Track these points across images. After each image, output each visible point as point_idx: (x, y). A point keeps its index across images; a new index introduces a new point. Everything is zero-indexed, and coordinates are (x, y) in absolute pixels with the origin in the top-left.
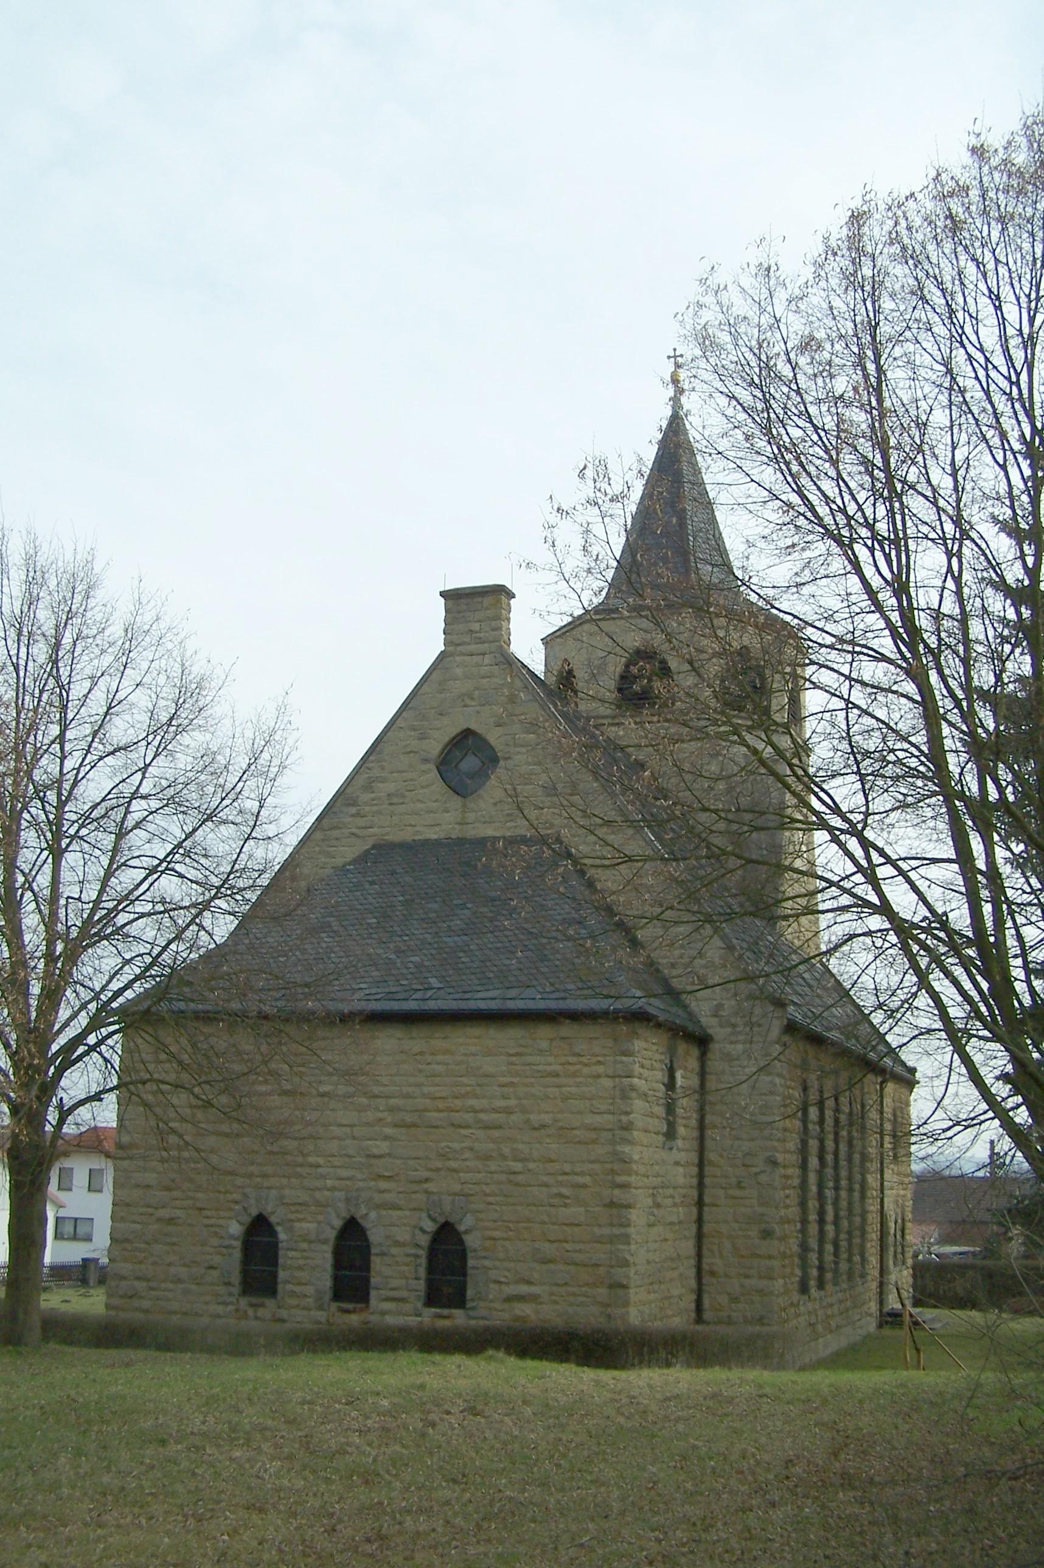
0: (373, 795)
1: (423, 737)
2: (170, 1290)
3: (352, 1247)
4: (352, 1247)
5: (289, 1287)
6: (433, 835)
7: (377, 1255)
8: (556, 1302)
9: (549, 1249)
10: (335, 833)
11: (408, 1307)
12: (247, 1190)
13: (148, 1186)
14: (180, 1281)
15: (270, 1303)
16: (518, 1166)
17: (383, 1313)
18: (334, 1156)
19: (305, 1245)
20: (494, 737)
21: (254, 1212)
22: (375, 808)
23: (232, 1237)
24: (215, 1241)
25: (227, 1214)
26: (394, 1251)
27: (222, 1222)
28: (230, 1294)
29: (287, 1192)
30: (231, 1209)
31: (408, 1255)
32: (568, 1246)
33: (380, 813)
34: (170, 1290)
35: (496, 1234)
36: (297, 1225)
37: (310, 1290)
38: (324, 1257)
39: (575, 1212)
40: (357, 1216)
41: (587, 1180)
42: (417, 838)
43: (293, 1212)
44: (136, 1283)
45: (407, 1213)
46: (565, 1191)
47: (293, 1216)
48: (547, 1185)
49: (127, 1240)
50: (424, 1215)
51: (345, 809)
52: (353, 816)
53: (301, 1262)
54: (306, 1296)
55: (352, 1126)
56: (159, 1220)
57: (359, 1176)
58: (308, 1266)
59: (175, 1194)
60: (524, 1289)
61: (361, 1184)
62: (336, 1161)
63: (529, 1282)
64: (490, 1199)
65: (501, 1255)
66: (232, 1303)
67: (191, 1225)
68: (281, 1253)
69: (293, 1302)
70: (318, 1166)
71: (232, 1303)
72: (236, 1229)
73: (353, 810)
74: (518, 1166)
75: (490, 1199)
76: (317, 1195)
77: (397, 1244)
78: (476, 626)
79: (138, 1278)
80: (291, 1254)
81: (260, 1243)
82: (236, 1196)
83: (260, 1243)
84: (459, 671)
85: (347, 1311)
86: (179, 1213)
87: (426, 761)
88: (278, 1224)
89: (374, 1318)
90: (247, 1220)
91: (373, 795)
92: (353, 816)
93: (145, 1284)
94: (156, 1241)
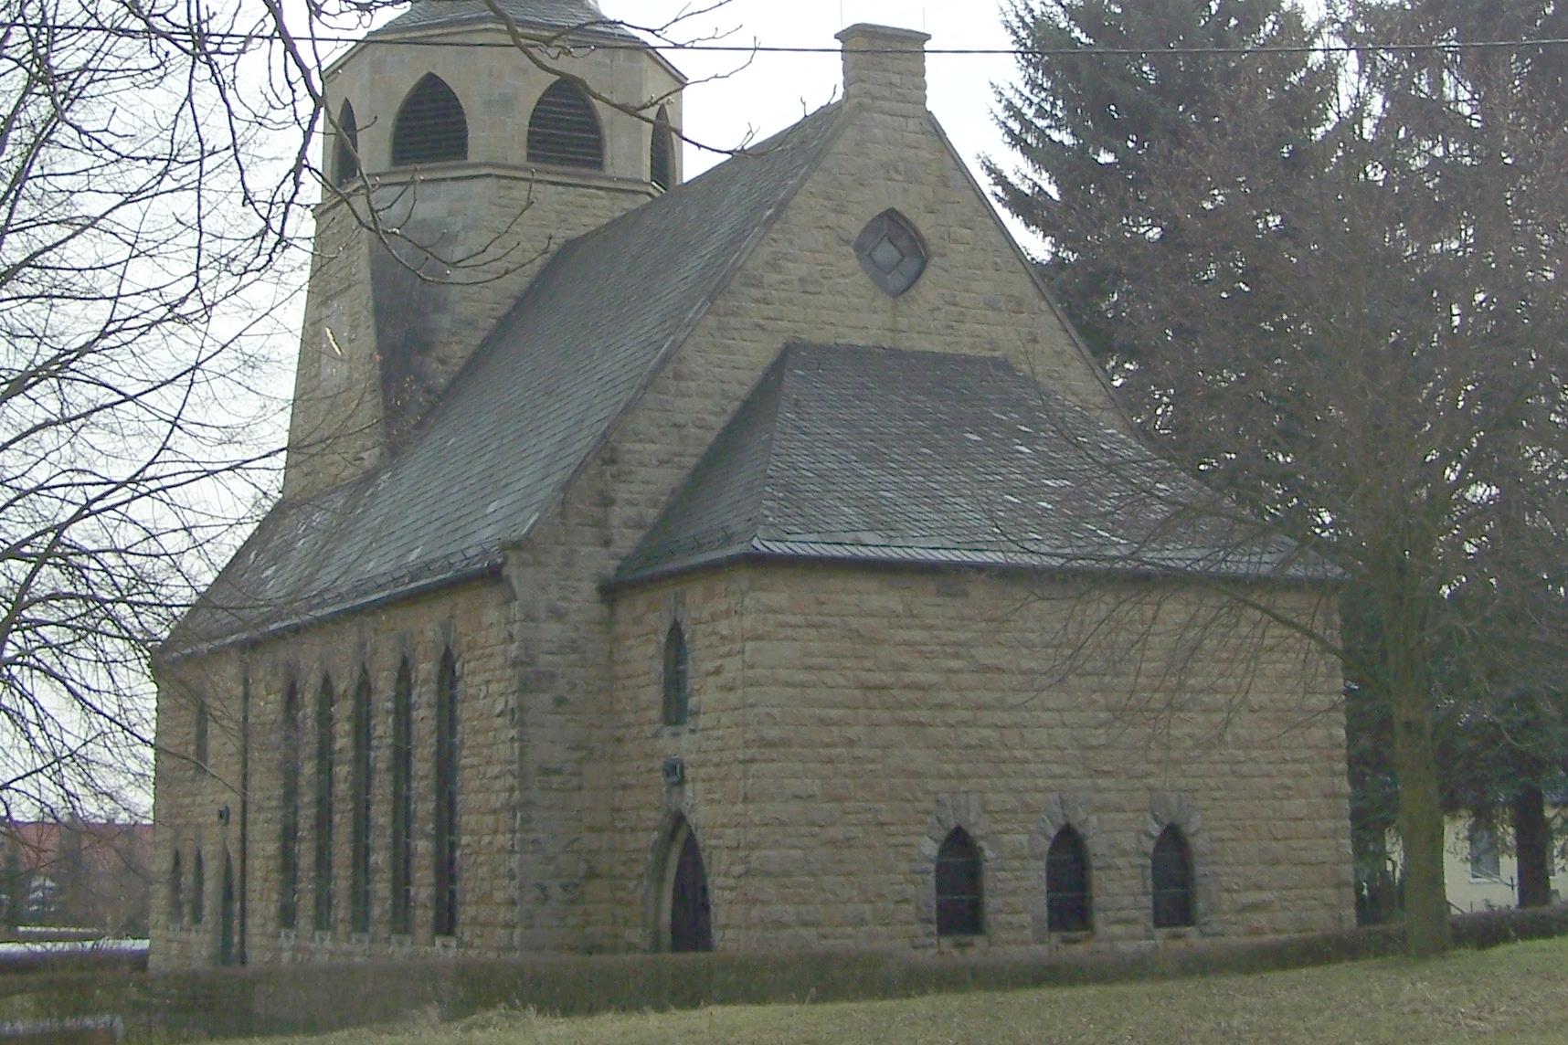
0: (781, 277)
1: (840, 210)
2: (850, 936)
3: (1069, 859)
4: (1069, 859)
5: (1000, 917)
6: (858, 340)
7: (1100, 869)
8: (1287, 909)
9: (1278, 847)
10: (733, 321)
11: (1139, 929)
12: (943, 796)
13: (812, 797)
14: (863, 922)
15: (979, 941)
16: (1240, 754)
17: (1111, 939)
18: (1042, 748)
19: (1017, 864)
20: (925, 225)
21: (953, 825)
22: (783, 295)
23: (927, 859)
24: (904, 866)
25: (918, 828)
26: (1120, 862)
27: (914, 839)
28: (930, 934)
29: (990, 796)
30: (922, 822)
31: (1132, 866)
32: (1294, 843)
33: (790, 301)
34: (850, 936)
35: (1226, 835)
36: (1006, 838)
37: (1026, 919)
38: (1037, 874)
39: (1297, 805)
40: (1074, 823)
41: (1306, 768)
42: (839, 341)
43: (997, 822)
44: (804, 932)
45: (1131, 815)
46: (1289, 782)
47: (998, 827)
48: (1269, 776)
49: (787, 873)
50: (1149, 817)
51: (744, 289)
52: (757, 301)
53: (1014, 884)
54: (1023, 927)
55: (1060, 711)
56: (831, 842)
57: (1074, 773)
58: (1017, 889)
59: (848, 805)
60: (1254, 896)
61: (1076, 782)
62: (1048, 755)
63: (1260, 888)
64: (1217, 794)
65: (1231, 860)
66: (931, 946)
67: (870, 847)
68: (988, 874)
69: (1004, 936)
70: (1027, 761)
71: (931, 946)
72: (930, 848)
73: (757, 293)
74: (1240, 754)
75: (1217, 794)
76: (1028, 798)
77: (1124, 853)
78: (896, 79)
79: (805, 924)
80: (1002, 875)
81: (960, 866)
82: (931, 806)
83: (960, 866)
84: (878, 133)
85: (1075, 941)
86: (857, 832)
87: (847, 242)
88: (982, 838)
89: (1104, 946)
90: (942, 834)
91: (781, 277)
92: (757, 301)
93: (813, 931)
94: (825, 873)
